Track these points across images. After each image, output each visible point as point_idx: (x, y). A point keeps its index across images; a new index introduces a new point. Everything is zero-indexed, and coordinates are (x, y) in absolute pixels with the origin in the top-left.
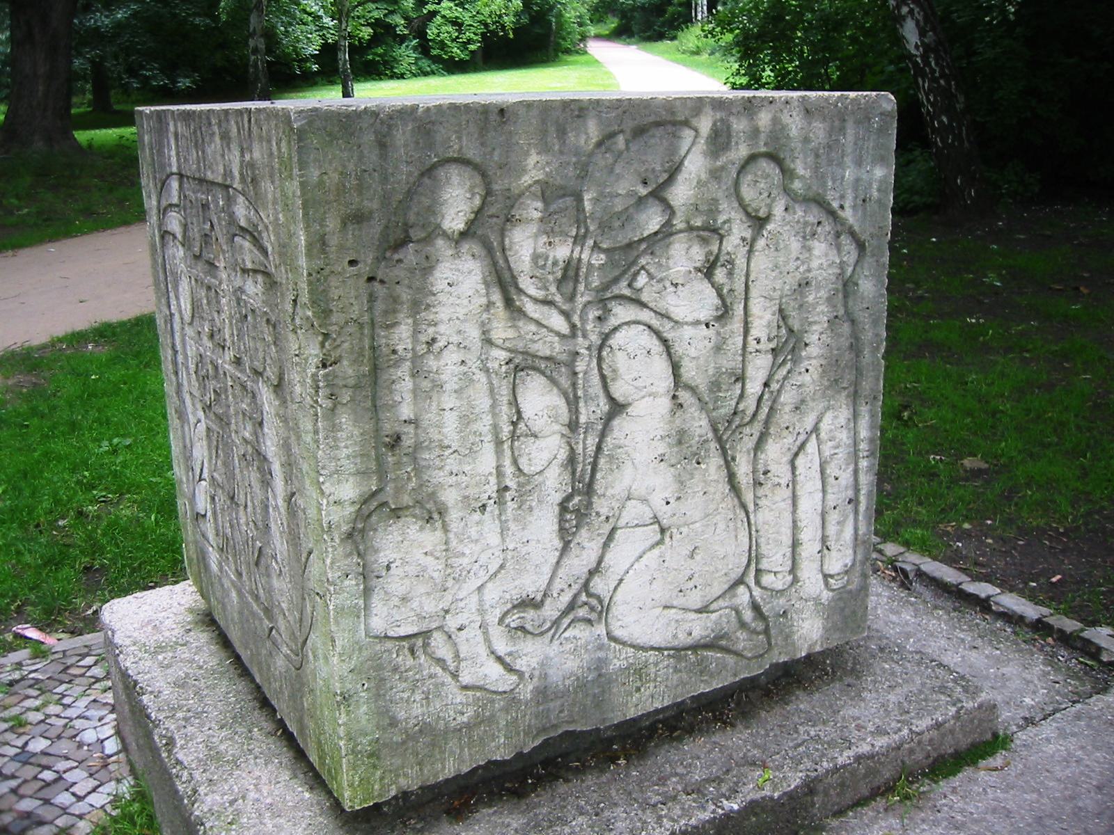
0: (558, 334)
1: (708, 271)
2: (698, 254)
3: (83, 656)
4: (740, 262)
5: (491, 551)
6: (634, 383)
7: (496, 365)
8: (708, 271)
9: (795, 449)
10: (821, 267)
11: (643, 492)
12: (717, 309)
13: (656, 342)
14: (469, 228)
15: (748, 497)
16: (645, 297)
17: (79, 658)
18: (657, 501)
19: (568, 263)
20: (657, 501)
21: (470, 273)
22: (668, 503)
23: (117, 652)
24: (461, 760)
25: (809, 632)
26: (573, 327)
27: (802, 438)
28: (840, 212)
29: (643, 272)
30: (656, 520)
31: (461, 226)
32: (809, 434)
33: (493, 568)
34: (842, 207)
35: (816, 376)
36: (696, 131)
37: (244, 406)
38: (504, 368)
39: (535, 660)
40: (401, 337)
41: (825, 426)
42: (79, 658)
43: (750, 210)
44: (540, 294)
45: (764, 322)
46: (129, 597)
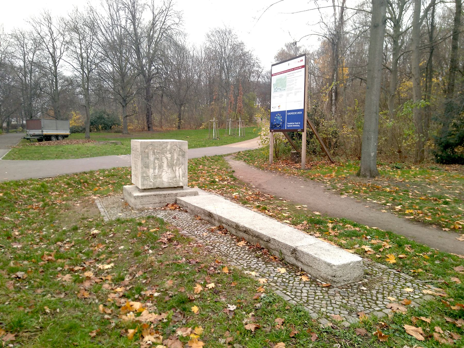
25: (181, 184)
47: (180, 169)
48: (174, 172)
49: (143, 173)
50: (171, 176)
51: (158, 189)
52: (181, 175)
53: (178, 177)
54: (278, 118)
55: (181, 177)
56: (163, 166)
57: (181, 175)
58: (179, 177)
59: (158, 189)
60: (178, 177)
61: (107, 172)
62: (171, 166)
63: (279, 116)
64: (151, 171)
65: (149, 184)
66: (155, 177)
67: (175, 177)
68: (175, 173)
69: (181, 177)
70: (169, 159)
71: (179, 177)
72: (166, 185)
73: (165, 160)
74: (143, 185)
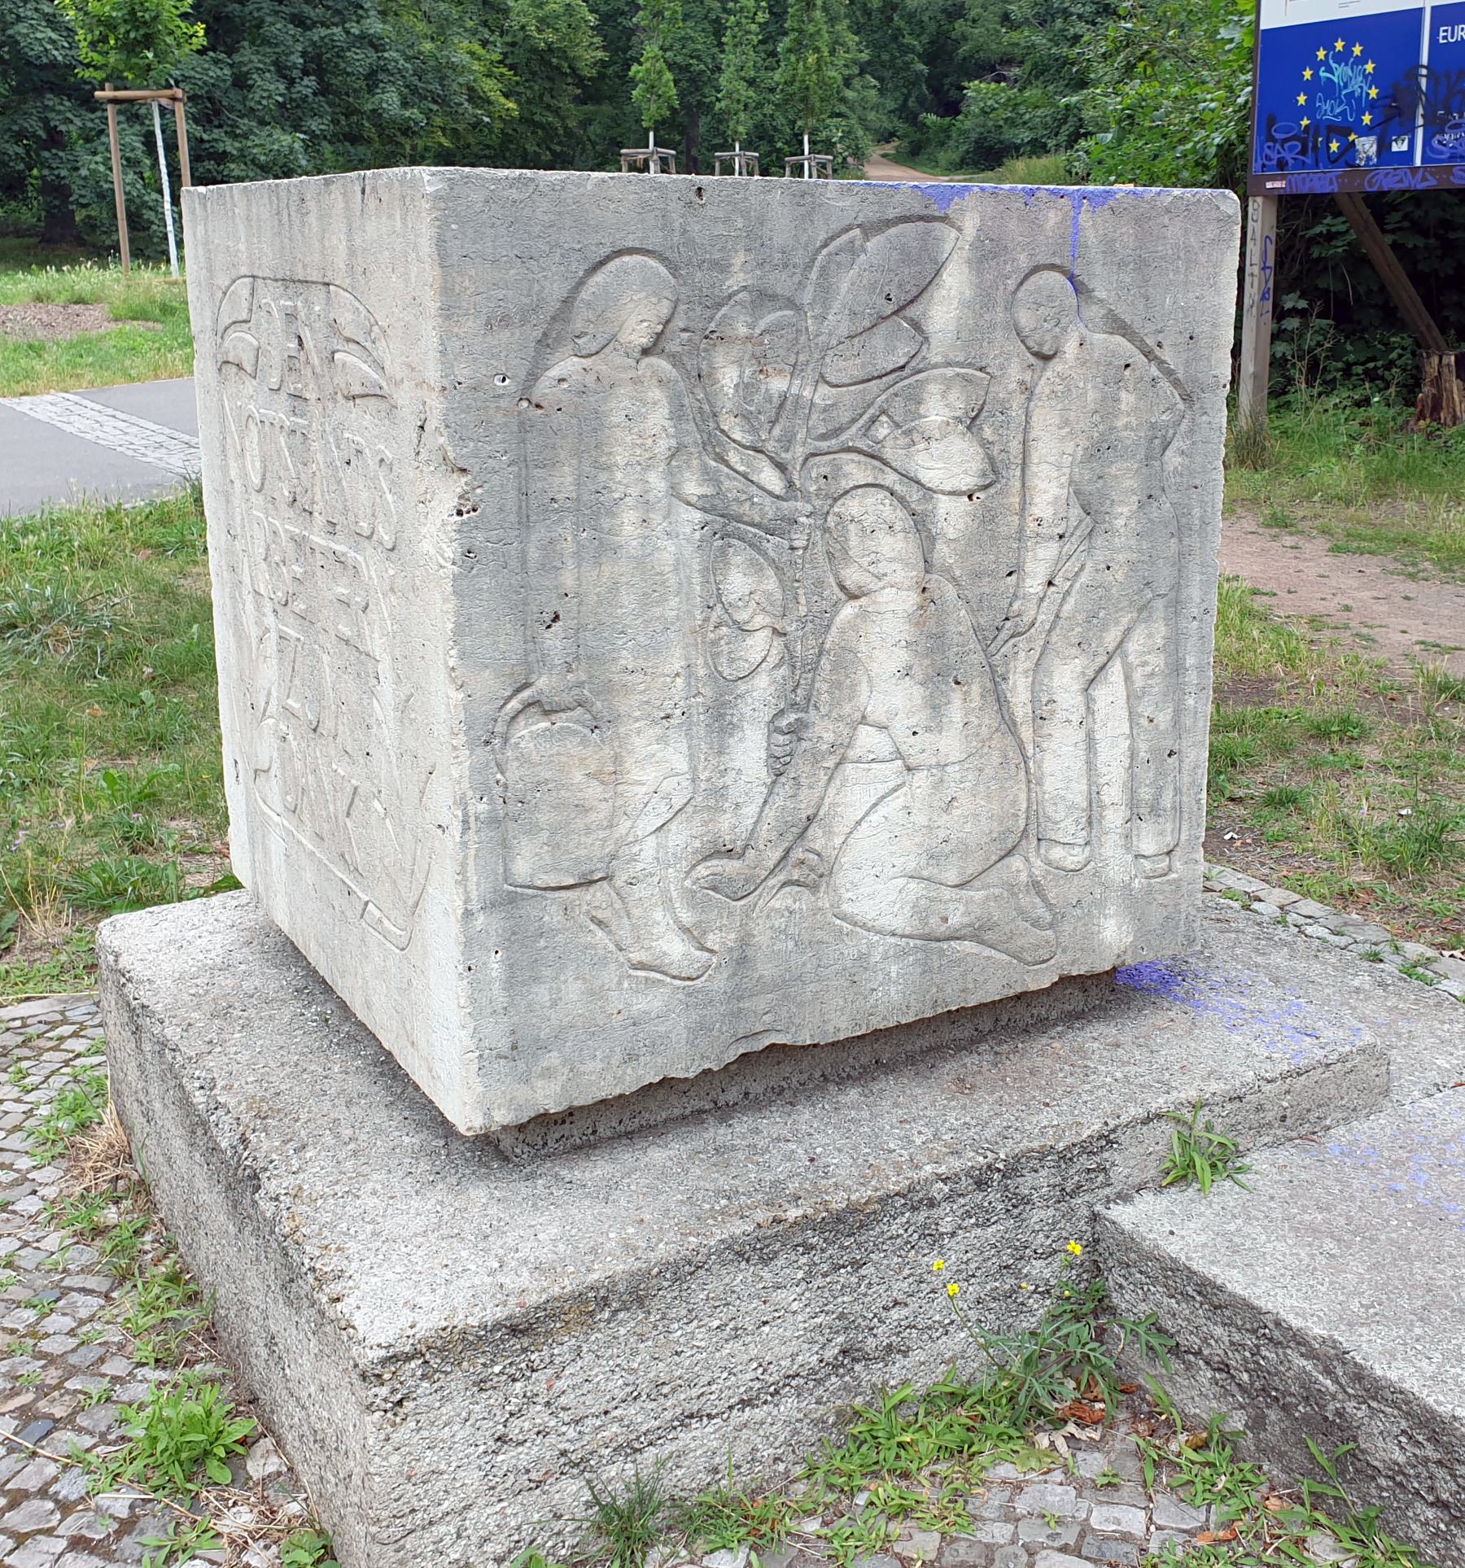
0: (770, 493)
1: (972, 423)
2: (958, 401)
3: (54, 1025)
4: (1016, 412)
5: (676, 779)
6: (871, 569)
7: (688, 530)
8: (972, 423)
9: (1091, 673)
10: (1126, 427)
11: (883, 719)
12: (984, 475)
13: (901, 513)
14: (655, 344)
15: (1026, 733)
16: (888, 453)
17: (47, 1027)
18: (900, 727)
19: (784, 398)
20: (900, 727)
21: (655, 404)
22: (915, 733)
23: (123, 980)
24: (619, 1080)
25: (1113, 938)
26: (790, 485)
27: (1102, 659)
28: (1157, 351)
29: (884, 418)
30: (899, 754)
31: (645, 341)
32: (1110, 657)
33: (678, 803)
34: (1160, 345)
35: (1120, 577)
36: (960, 230)
37: (341, 590)
38: (697, 535)
39: (732, 936)
40: (563, 481)
41: (1132, 647)
42: (47, 1027)
43: (1031, 343)
44: (747, 439)
45: (1048, 497)
46: (142, 912)
47: (1111, 693)
48: (1011, 737)
49: (502, 816)
50: (973, 819)
51: (774, 1073)
52: (1113, 794)
53: (1068, 827)
54: (1340, 73)
55: (1114, 818)
56: (847, 661)
57: (1113, 794)
58: (1092, 818)
59: (774, 1073)
60: (1068, 827)
61: (289, 798)
62: (974, 647)
63: (1343, 57)
64: (658, 765)
65: (643, 1005)
66: (727, 871)
67: (1026, 833)
68: (1023, 763)
69: (1114, 818)
70: (952, 517)
71: (1092, 818)
72: (893, 995)
73: (883, 554)
74: (518, 1052)
